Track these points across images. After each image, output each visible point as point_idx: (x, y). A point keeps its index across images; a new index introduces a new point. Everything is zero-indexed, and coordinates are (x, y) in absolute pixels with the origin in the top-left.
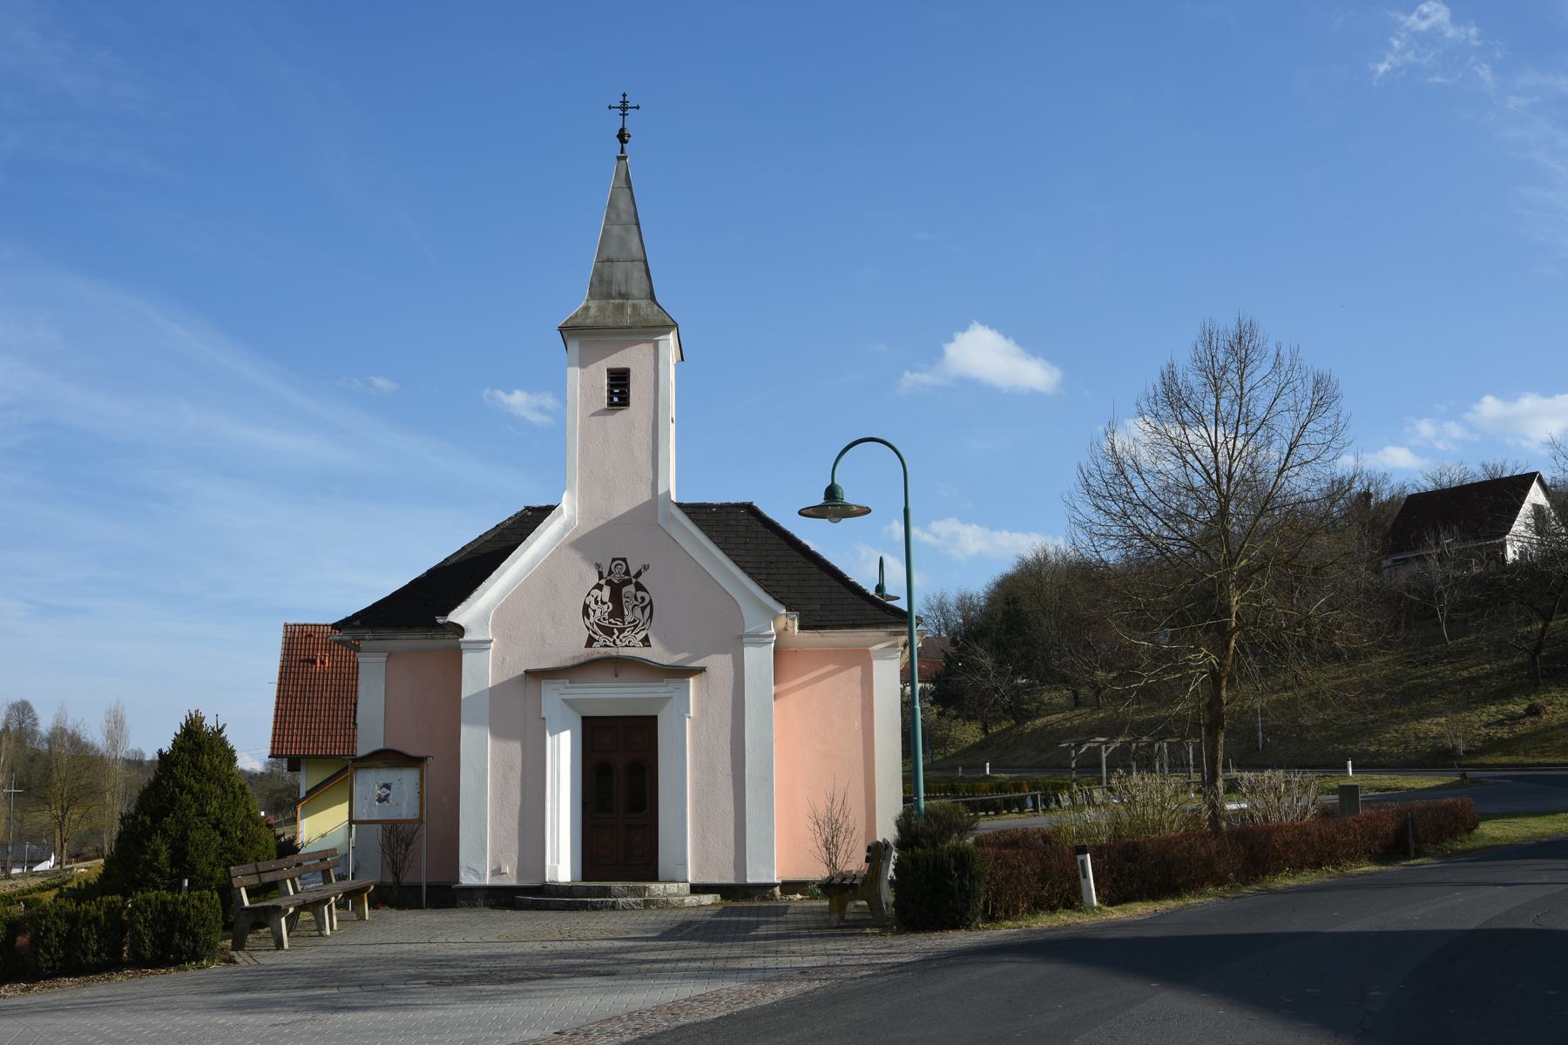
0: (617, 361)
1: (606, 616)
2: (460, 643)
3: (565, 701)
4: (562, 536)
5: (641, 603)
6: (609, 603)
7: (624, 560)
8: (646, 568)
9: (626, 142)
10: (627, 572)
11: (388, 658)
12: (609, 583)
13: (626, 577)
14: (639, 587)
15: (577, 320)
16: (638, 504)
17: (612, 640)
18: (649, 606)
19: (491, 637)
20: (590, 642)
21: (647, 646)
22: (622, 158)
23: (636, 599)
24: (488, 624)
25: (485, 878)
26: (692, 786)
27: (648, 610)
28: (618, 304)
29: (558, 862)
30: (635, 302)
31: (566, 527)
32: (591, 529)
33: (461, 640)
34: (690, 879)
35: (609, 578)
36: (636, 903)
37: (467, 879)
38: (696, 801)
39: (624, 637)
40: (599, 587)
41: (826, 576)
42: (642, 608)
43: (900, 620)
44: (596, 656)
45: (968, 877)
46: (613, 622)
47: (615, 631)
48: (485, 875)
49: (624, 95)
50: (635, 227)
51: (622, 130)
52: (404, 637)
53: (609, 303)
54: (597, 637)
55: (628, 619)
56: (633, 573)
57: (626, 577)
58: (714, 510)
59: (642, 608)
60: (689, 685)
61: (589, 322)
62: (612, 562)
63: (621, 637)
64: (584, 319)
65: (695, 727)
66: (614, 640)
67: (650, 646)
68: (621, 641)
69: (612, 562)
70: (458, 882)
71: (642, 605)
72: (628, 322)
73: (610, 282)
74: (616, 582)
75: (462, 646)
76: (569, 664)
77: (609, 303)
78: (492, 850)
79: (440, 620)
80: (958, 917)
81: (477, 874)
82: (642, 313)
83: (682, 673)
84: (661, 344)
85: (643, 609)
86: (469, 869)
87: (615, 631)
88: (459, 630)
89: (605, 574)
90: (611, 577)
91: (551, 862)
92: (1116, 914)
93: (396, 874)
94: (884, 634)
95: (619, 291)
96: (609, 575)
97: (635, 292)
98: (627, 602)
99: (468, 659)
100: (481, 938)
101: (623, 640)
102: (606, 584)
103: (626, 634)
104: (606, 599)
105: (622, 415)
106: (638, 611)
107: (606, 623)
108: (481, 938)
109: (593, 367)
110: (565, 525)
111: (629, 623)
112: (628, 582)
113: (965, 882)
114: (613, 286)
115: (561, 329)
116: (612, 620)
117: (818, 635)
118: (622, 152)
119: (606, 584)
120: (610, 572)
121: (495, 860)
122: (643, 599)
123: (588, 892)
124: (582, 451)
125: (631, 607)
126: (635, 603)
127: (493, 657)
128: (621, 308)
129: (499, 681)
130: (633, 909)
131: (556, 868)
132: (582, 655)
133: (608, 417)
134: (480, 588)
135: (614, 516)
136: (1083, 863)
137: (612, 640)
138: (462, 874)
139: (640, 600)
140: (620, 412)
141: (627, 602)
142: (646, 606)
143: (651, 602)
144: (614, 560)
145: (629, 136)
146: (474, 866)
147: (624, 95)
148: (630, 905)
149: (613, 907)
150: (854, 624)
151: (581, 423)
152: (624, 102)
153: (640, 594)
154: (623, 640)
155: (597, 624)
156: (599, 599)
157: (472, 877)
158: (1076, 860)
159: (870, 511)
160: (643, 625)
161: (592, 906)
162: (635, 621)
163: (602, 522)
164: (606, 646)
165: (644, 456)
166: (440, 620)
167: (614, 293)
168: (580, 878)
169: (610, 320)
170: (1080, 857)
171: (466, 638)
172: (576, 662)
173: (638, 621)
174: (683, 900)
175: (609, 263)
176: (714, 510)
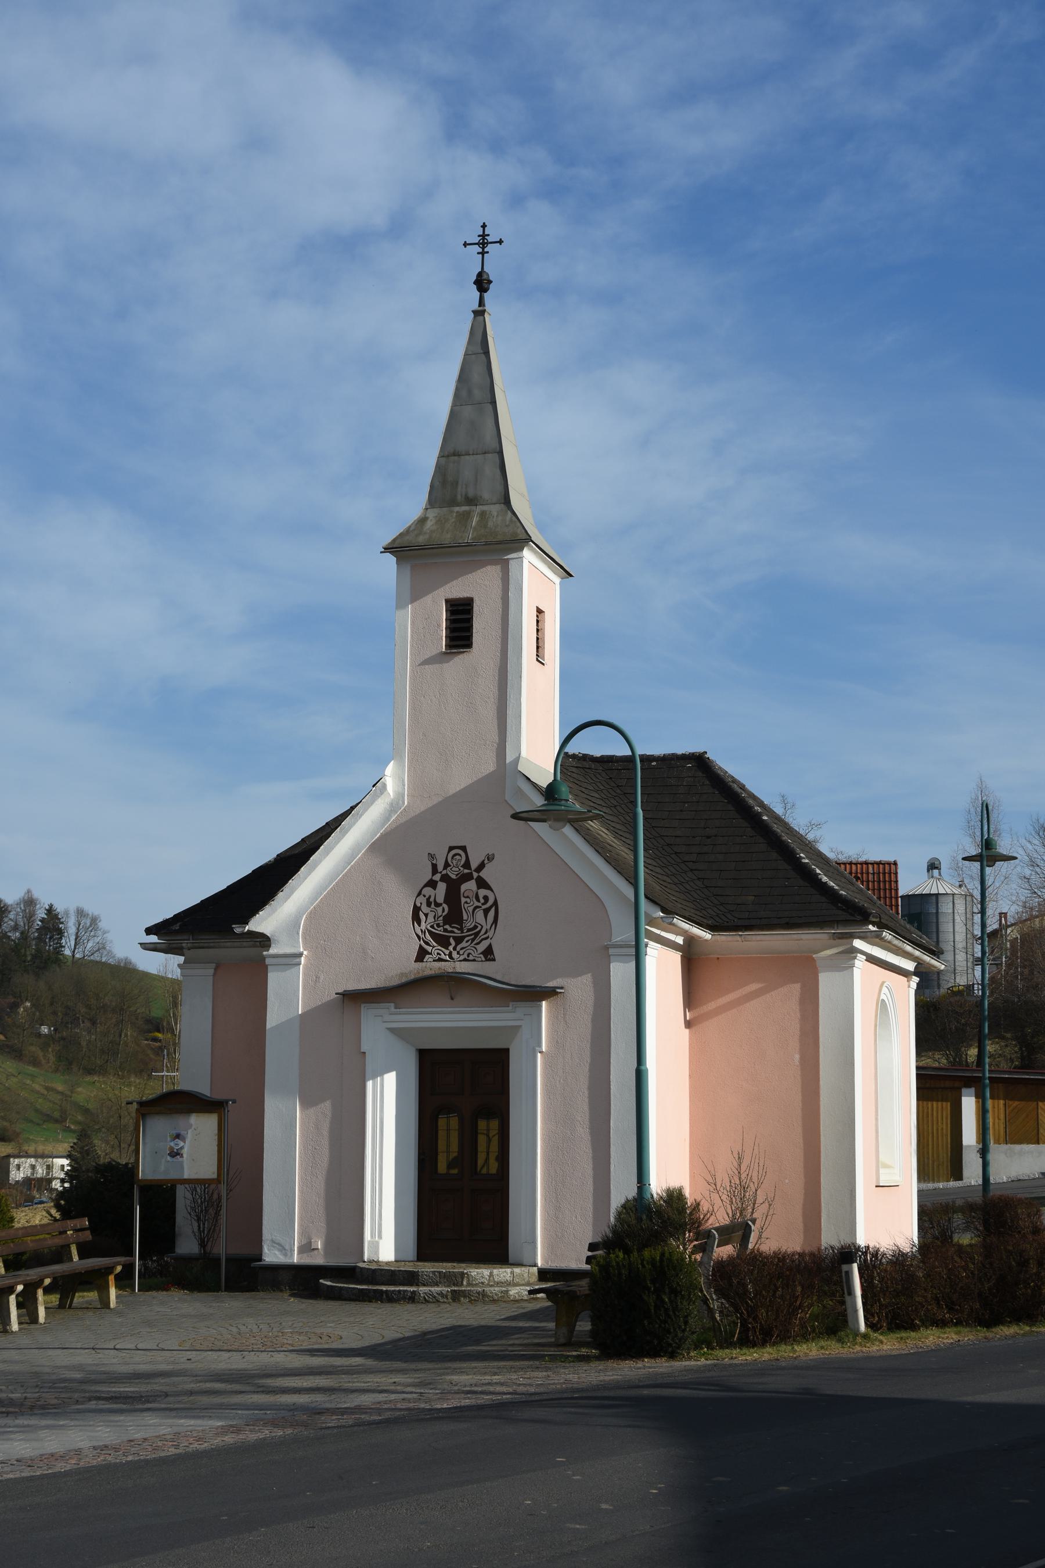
0: (457, 589)
1: (440, 921)
2: (264, 958)
3: (392, 1030)
4: (388, 819)
5: (483, 904)
6: (445, 906)
7: (464, 848)
8: (490, 858)
9: (486, 290)
10: (467, 865)
11: (216, 969)
12: (445, 878)
13: (466, 871)
14: (482, 884)
15: (407, 538)
16: (480, 776)
17: (447, 952)
18: (493, 909)
19: (302, 950)
20: (421, 955)
21: (490, 960)
22: (479, 313)
23: (478, 900)
24: (298, 934)
25: (292, 1255)
26: (543, 1140)
27: (492, 913)
28: (464, 511)
29: (380, 1237)
30: (485, 508)
31: (393, 807)
32: (423, 809)
33: (265, 953)
34: (539, 1265)
35: (444, 872)
36: (441, 1294)
37: (271, 1256)
38: (548, 1162)
39: (462, 949)
40: (432, 884)
41: (774, 855)
42: (484, 910)
43: (852, 918)
44: (428, 973)
45: (667, 1291)
46: (449, 929)
47: (452, 941)
48: (292, 1250)
49: (484, 226)
50: (490, 407)
51: (480, 275)
52: (229, 944)
53: (452, 512)
54: (429, 949)
55: (469, 925)
56: (474, 865)
57: (466, 871)
58: (654, 763)
59: (484, 910)
60: (540, 1011)
61: (421, 539)
62: (449, 852)
63: (458, 948)
64: (417, 536)
65: (548, 1065)
66: (451, 953)
67: (494, 960)
68: (458, 953)
69: (449, 852)
70: (260, 1260)
71: (484, 907)
72: (470, 536)
73: (455, 484)
74: (454, 877)
75: (268, 961)
76: (396, 982)
77: (452, 512)
78: (301, 1218)
79: (238, 929)
80: (656, 1342)
81: (282, 1249)
82: (490, 524)
83: (534, 994)
84: (512, 565)
85: (486, 912)
86: (275, 1243)
87: (452, 941)
88: (263, 941)
89: (440, 868)
90: (448, 871)
91: (372, 1237)
92: (888, 1345)
93: (203, 1244)
94: (825, 936)
95: (466, 495)
96: (445, 868)
97: (486, 495)
98: (466, 902)
99: (275, 979)
100: (158, 1346)
101: (461, 952)
102: (441, 880)
103: (464, 944)
104: (440, 899)
105: (461, 661)
106: (480, 915)
107: (439, 931)
108: (158, 1346)
109: (428, 599)
110: (391, 804)
111: (469, 930)
112: (468, 877)
113: (664, 1297)
114: (459, 489)
115: (399, 549)
116: (447, 927)
117: (738, 938)
118: (480, 305)
119: (441, 880)
120: (447, 865)
121: (304, 1232)
122: (486, 898)
123: (412, 1278)
124: (414, 708)
125: (471, 909)
126: (477, 904)
127: (304, 974)
128: (466, 517)
129: (309, 1008)
130: (438, 1301)
131: (378, 1243)
132: (410, 972)
133: (445, 665)
134: (287, 888)
135: (452, 792)
136: (849, 1275)
137: (447, 952)
138: (266, 1249)
139: (482, 901)
140: (461, 656)
141: (466, 902)
142: (491, 907)
143: (496, 903)
144: (451, 848)
145: (490, 282)
146: (279, 1238)
147: (484, 226)
148: (435, 1297)
149: (412, 1298)
150: (787, 923)
151: (412, 671)
152: (484, 236)
153: (482, 892)
154: (461, 952)
155: (429, 932)
156: (432, 899)
157: (277, 1252)
158: (841, 1271)
159: (429, 854)
160: (486, 933)
161: (387, 1296)
162: (475, 927)
163: (436, 800)
164: (440, 960)
165: (488, 712)
166: (238, 929)
167: (459, 497)
168: (411, 1252)
169: (449, 536)
170: (845, 1267)
171: (273, 950)
172: (404, 980)
173: (480, 927)
174: (507, 1291)
175: (456, 458)
176: (654, 763)
